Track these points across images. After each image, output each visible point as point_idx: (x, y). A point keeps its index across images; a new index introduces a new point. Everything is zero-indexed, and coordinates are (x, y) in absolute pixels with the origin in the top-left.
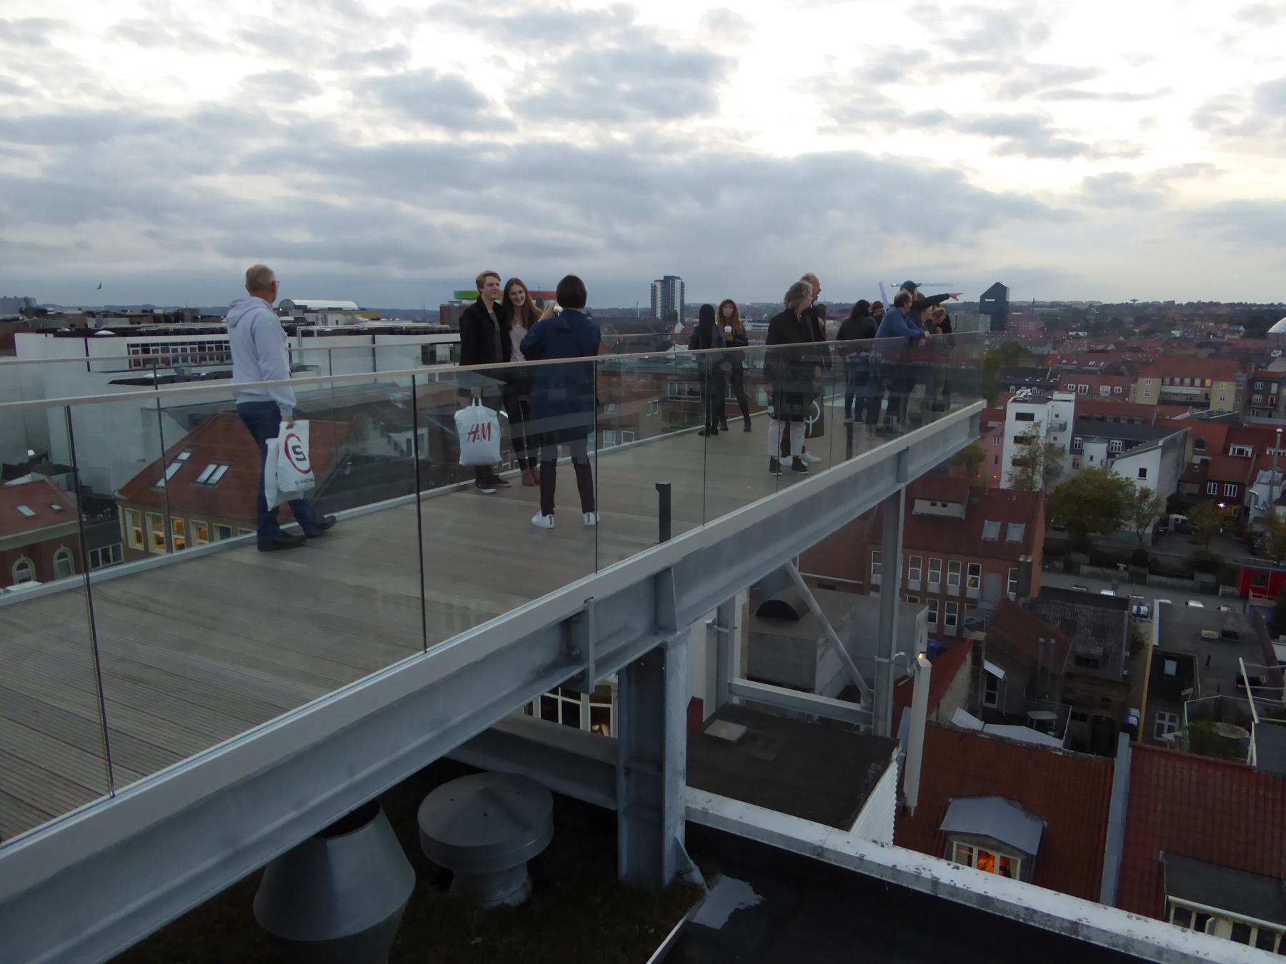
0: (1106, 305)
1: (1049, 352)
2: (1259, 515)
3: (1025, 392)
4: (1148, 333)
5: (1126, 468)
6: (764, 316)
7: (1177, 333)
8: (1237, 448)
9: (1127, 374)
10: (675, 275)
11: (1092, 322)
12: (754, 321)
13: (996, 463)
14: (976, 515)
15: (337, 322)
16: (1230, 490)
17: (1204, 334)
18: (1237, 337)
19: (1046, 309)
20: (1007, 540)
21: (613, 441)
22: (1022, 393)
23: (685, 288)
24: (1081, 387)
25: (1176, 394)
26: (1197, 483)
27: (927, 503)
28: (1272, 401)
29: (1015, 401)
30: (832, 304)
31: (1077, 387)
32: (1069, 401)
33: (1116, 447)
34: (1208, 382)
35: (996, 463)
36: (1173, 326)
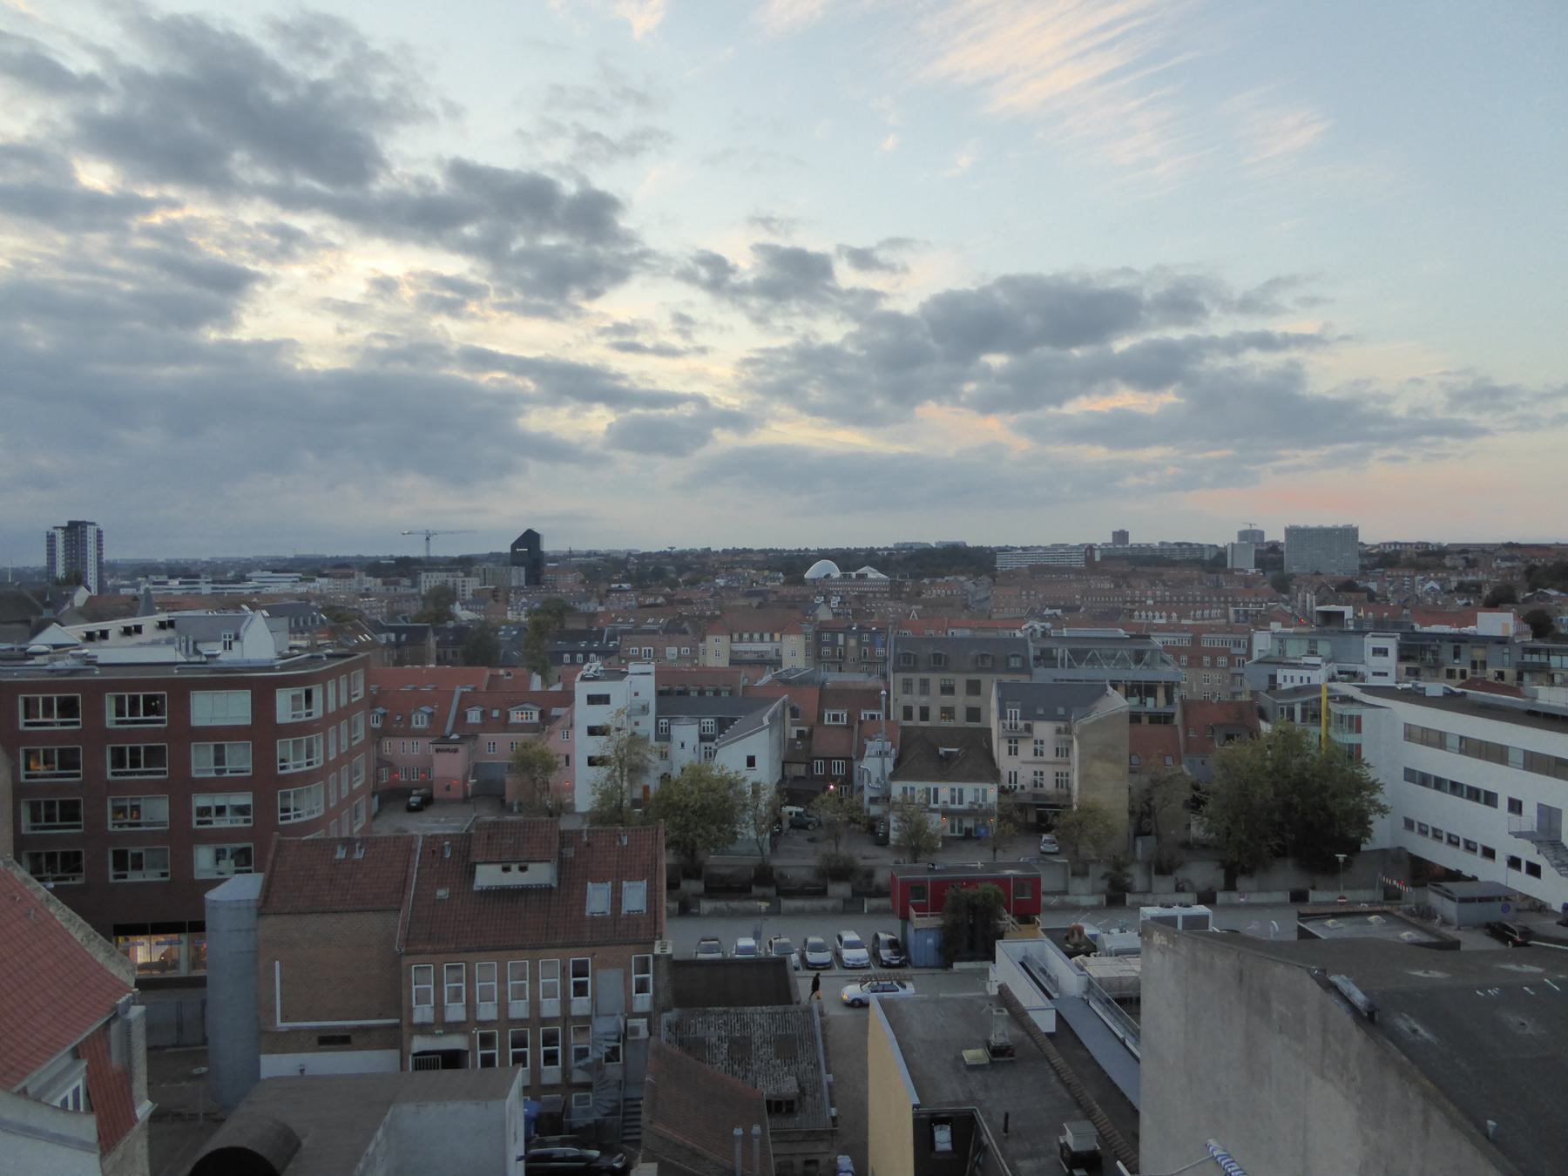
0: (644, 554)
1: (596, 609)
2: (874, 794)
3: (596, 665)
4: (693, 583)
5: (730, 759)
6: (228, 575)
7: (721, 582)
8: (831, 713)
9: (689, 630)
10: (87, 520)
11: (633, 572)
12: (213, 582)
13: (567, 764)
14: (572, 876)
16: (838, 770)
17: (748, 581)
18: (778, 584)
19: (583, 559)
20: (624, 911)
22: (591, 667)
24: (645, 650)
25: (746, 652)
26: (803, 763)
27: (497, 868)
28: (840, 653)
29: (584, 679)
30: (326, 559)
31: (640, 651)
32: (649, 674)
33: (708, 727)
34: (777, 636)
35: (567, 764)
36: (715, 574)
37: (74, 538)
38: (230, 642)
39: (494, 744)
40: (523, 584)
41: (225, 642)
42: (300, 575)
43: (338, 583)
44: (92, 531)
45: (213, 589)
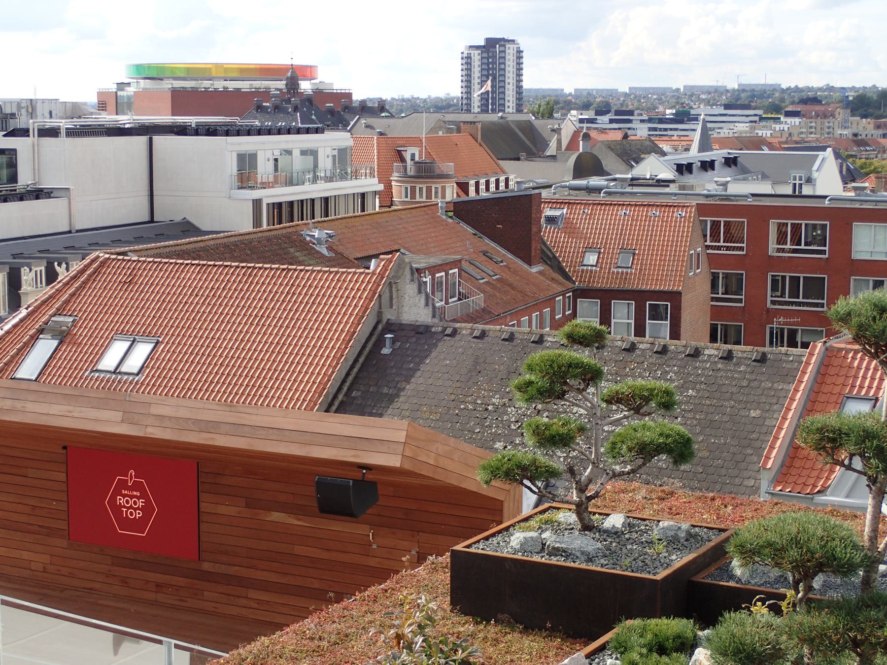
12: (650, 120)
15: (51, 113)
23: (524, 60)
37: (490, 60)
38: (801, 185)
43: (813, 124)
44: (511, 51)
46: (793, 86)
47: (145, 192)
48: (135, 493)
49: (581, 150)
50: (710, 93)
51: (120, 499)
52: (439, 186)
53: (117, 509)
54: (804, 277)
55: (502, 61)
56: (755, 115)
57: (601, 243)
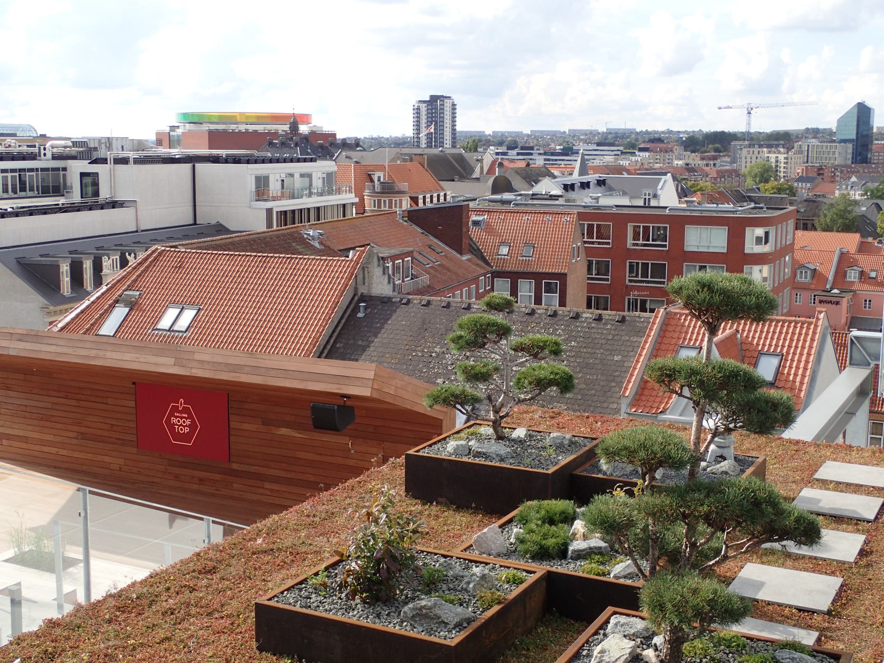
12: (545, 154)
15: (122, 147)
21: (708, 228)
38: (649, 199)
39: (870, 301)
40: (849, 162)
41: (645, 199)
42: (621, 148)
44: (448, 105)
45: (545, 160)
46: (644, 130)
47: (191, 204)
48: (184, 415)
49: (497, 174)
50: (587, 135)
51: (173, 419)
52: (397, 199)
53: (171, 426)
54: (651, 263)
55: (442, 111)
56: (618, 150)
57: (511, 239)
